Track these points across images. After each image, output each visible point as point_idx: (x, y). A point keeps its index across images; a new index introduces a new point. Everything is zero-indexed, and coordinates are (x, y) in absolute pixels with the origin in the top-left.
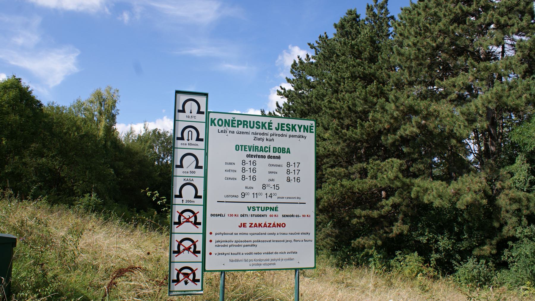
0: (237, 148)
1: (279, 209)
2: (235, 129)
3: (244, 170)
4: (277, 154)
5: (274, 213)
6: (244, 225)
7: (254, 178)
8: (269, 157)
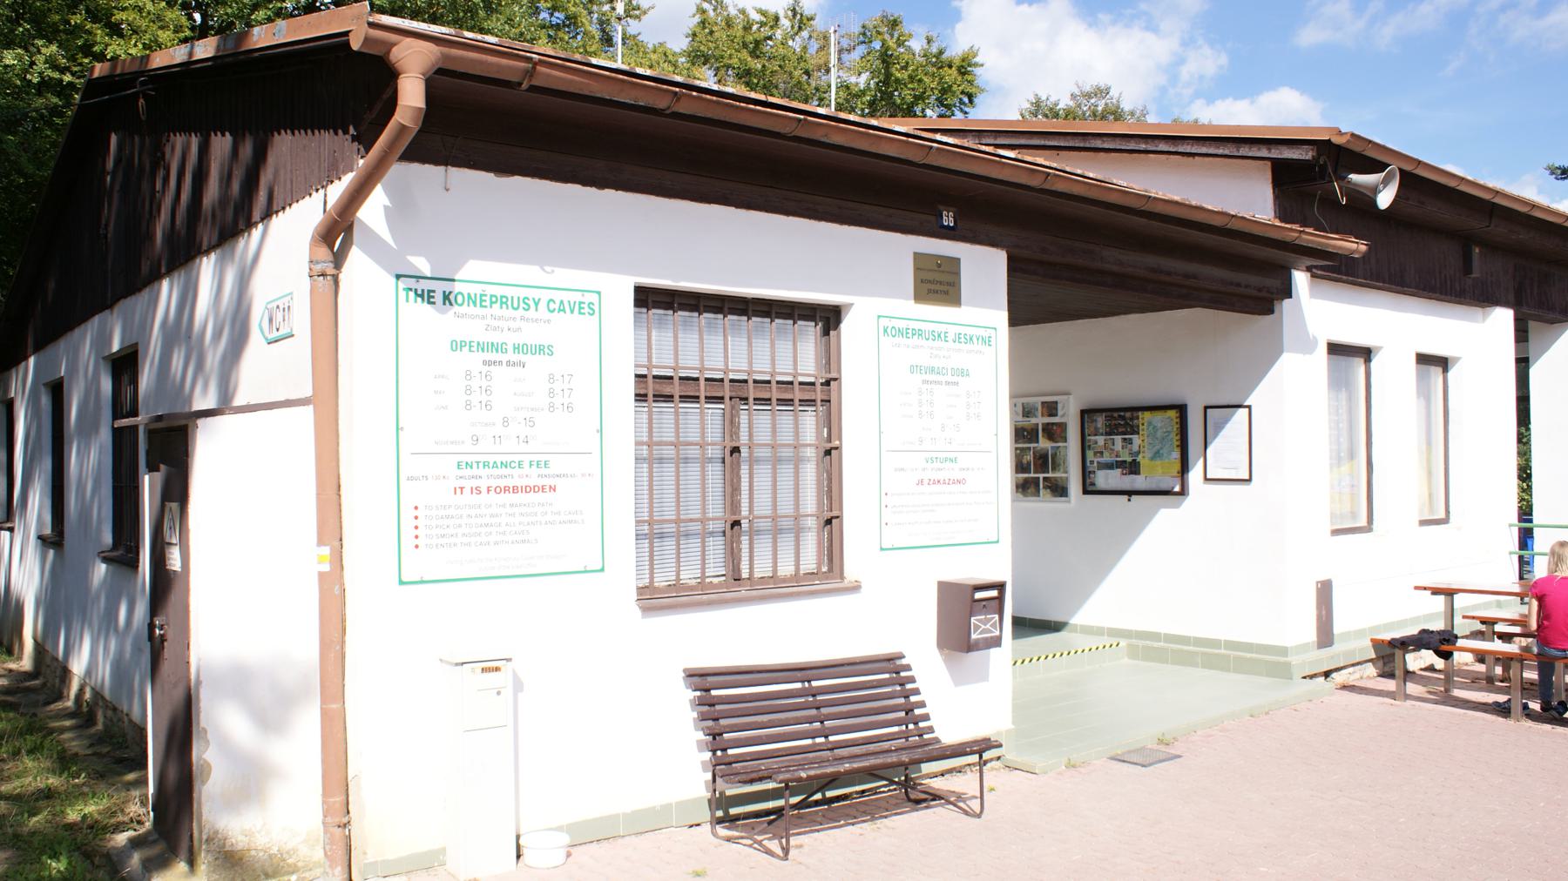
0: (457, 346)
1: (550, 464)
2: (909, 342)
3: (920, 404)
4: (955, 379)
5: (952, 465)
6: (921, 482)
7: (488, 406)
8: (948, 383)
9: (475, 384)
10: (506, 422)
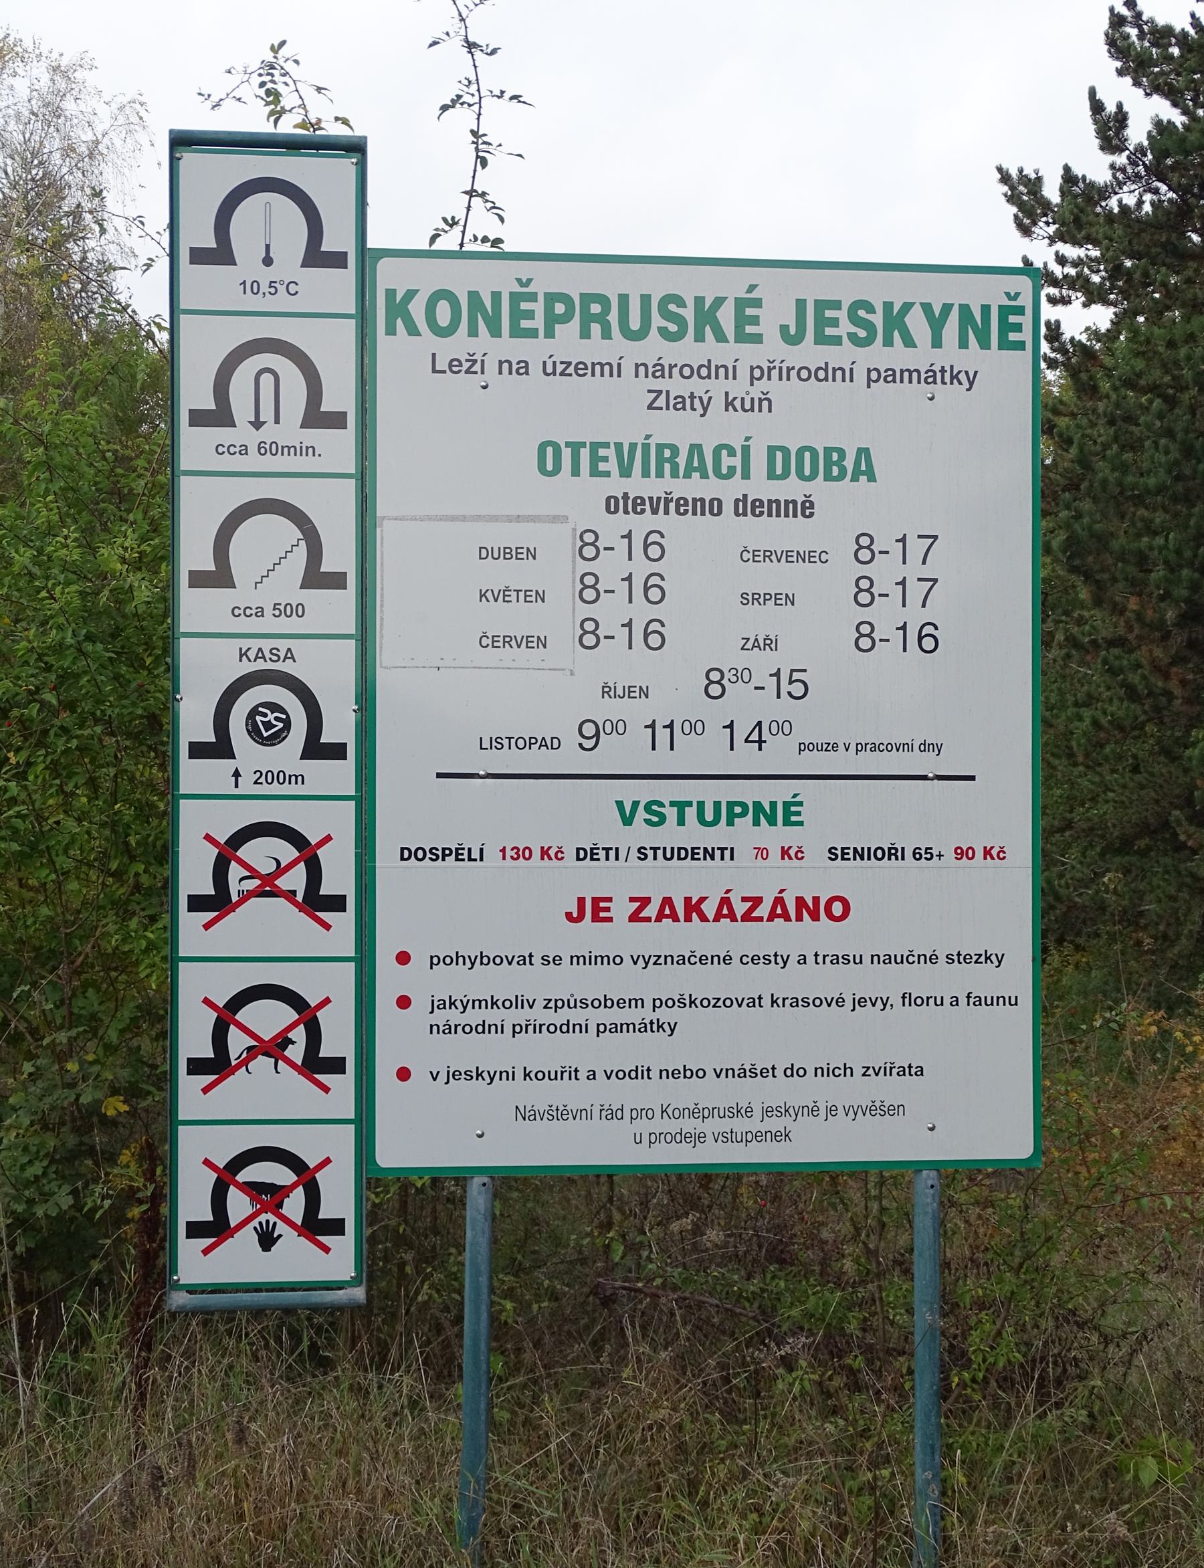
0: (549, 457)
2: (534, 351)
3: (589, 588)
5: (776, 836)
6: (599, 909)
7: (653, 636)
9: (610, 569)
10: (715, 683)
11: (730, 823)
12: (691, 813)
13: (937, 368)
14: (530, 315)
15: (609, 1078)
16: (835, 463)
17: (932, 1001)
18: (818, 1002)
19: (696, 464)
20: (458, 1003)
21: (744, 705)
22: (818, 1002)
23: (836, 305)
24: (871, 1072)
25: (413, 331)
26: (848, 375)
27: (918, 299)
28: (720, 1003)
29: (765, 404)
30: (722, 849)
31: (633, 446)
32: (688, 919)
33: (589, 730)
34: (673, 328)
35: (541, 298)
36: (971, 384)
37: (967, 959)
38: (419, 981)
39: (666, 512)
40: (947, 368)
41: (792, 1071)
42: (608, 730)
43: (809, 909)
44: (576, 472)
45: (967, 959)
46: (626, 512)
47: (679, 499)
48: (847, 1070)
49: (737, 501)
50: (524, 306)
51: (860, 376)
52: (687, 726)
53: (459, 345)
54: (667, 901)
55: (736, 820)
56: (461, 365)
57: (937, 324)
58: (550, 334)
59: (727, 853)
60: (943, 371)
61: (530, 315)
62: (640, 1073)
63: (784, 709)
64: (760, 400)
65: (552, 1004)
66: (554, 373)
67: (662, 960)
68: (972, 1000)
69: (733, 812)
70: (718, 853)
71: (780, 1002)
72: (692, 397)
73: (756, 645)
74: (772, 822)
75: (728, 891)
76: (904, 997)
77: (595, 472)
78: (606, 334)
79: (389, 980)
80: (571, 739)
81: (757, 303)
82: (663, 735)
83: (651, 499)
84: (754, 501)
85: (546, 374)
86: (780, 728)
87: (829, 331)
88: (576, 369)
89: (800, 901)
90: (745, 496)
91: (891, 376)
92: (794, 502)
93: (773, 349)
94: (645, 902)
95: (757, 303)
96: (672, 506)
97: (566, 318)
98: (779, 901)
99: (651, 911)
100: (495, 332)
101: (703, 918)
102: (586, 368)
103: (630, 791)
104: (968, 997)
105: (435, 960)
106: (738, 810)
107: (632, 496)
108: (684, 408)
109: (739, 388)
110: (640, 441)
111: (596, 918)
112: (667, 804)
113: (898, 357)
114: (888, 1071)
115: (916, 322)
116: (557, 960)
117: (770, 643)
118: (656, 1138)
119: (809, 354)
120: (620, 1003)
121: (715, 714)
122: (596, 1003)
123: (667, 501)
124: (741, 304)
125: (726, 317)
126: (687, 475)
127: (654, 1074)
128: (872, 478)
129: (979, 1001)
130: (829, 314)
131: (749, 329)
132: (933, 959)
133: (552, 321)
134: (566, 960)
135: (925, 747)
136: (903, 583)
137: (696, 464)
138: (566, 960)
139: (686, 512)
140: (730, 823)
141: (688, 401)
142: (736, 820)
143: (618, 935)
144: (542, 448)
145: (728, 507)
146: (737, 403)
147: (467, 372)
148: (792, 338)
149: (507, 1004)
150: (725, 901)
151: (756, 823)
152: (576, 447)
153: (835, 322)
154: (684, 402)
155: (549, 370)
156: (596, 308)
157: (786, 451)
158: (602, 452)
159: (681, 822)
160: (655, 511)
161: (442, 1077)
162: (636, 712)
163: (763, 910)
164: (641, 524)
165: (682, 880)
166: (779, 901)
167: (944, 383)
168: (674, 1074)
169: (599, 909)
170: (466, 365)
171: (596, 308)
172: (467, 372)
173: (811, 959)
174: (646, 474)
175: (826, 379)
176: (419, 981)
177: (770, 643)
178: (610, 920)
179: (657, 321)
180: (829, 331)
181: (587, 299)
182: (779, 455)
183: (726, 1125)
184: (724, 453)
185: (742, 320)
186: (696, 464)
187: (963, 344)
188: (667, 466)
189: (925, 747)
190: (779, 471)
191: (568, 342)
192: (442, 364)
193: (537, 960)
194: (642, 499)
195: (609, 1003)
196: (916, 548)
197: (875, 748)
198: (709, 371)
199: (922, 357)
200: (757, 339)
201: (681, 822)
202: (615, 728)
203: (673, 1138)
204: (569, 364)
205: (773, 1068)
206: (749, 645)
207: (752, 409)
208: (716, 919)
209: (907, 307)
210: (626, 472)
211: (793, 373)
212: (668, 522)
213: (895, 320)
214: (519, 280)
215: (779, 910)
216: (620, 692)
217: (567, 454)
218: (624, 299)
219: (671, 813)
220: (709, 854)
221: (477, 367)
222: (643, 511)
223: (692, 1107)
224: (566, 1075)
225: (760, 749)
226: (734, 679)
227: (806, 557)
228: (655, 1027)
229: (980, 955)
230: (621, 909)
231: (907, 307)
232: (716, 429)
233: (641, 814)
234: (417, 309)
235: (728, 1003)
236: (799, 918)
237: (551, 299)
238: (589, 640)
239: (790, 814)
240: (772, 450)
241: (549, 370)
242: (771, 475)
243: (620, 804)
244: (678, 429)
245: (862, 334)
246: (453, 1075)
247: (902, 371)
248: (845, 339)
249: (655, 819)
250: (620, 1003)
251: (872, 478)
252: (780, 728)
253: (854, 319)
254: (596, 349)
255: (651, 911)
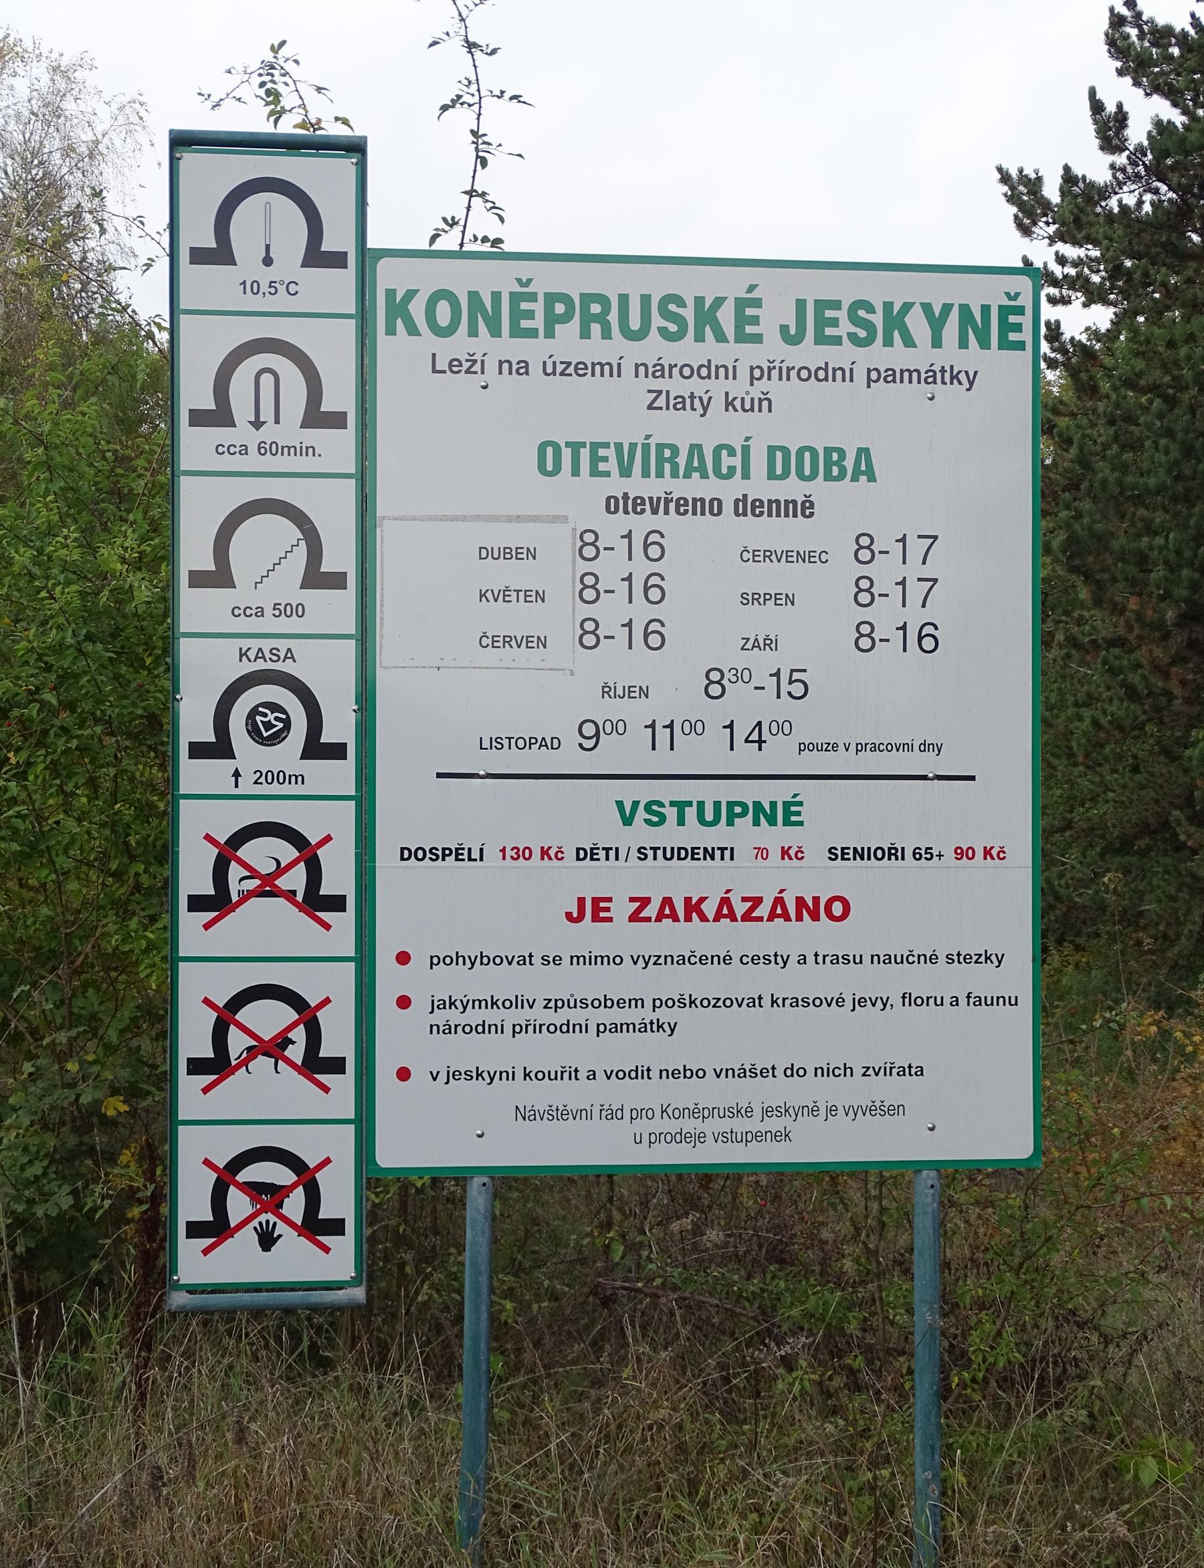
0: (549, 457)
2: (534, 351)
3: (589, 588)
5: (776, 836)
6: (599, 909)
7: (653, 636)
9: (610, 569)
10: (715, 683)
11: (730, 823)
12: (691, 813)
13: (937, 368)
14: (530, 315)
15: (609, 1078)
16: (835, 463)
17: (932, 1001)
18: (818, 1002)
19: (696, 464)
20: (458, 1003)
21: (744, 705)
22: (818, 1002)
23: (836, 305)
24: (871, 1072)
25: (413, 331)
26: (848, 375)
27: (918, 299)
28: (720, 1003)
29: (765, 404)
30: (722, 849)
31: (633, 446)
32: (688, 919)
33: (589, 730)
34: (673, 328)
35: (541, 298)
36: (971, 384)
37: (967, 959)
38: (419, 981)
39: (666, 512)
40: (947, 368)
41: (792, 1071)
42: (608, 730)
43: (809, 909)
44: (576, 472)
45: (967, 959)
46: (626, 512)
47: (679, 499)
48: (847, 1070)
49: (737, 501)
50: (524, 306)
51: (860, 376)
52: (687, 726)
53: (459, 345)
54: (667, 901)
55: (736, 820)
56: (461, 365)
57: (937, 324)
58: (550, 334)
59: (727, 853)
60: (943, 371)
61: (530, 315)
62: (640, 1073)
63: (784, 709)
64: (760, 400)
65: (552, 1004)
66: (554, 373)
67: (662, 960)
68: (972, 1000)
69: (733, 812)
70: (718, 853)
71: (780, 1002)
72: (692, 397)
73: (756, 645)
74: (772, 822)
75: (728, 891)
76: (904, 997)
77: (595, 472)
78: (606, 334)
79: (389, 980)
80: (571, 739)
81: (757, 303)
82: (663, 735)
83: (651, 499)
84: (754, 501)
85: (546, 374)
86: (780, 728)
87: (829, 331)
88: (576, 369)
89: (800, 901)
90: (745, 496)
91: (891, 376)
92: (794, 502)
93: (773, 349)
94: (645, 902)
95: (757, 303)
96: (672, 506)
97: (566, 318)
98: (779, 901)
99: (651, 911)
100: (495, 332)
101: (703, 918)
102: (586, 368)
103: (630, 791)
104: (968, 997)
105: (435, 960)
106: (738, 810)
107: (632, 496)
108: (684, 408)
109: (739, 388)
110: (640, 441)
111: (596, 918)
112: (667, 804)
113: (898, 357)
114: (888, 1071)
115: (916, 322)
116: (557, 960)
117: (770, 643)
118: (656, 1138)
119: (809, 354)
120: (620, 1003)
121: (715, 714)
122: (596, 1003)
123: (667, 501)
124: (741, 304)
125: (726, 317)
126: (687, 475)
127: (654, 1074)
128: (872, 478)
129: (979, 1001)
130: (829, 314)
131: (749, 329)
132: (933, 959)
133: (552, 321)
134: (566, 960)
135: (925, 747)
136: (903, 583)
137: (696, 464)
138: (566, 960)
139: (686, 512)
140: (730, 823)
141: (688, 401)
142: (736, 820)
143: (618, 935)
144: (542, 448)
145: (728, 507)
146: (737, 403)
147: (467, 372)
148: (792, 338)
149: (507, 1004)
150: (725, 901)
151: (756, 823)
152: (576, 447)
153: (835, 322)
154: (684, 402)
155: (549, 370)
156: (596, 308)
157: (786, 451)
158: (602, 452)
159: (681, 822)
160: (655, 511)
161: (442, 1077)
162: (636, 712)
163: (763, 910)
164: (641, 524)
165: (682, 880)
166: (779, 901)
167: (944, 383)
168: (674, 1074)
169: (599, 909)
170: (466, 365)
171: (596, 308)
172: (467, 372)
173: (811, 959)
174: (646, 474)
175: (826, 379)
176: (419, 981)
177: (770, 643)
178: (610, 920)
179: (657, 321)
180: (829, 331)
181: (587, 299)
182: (779, 455)
183: (726, 1125)
184: (724, 453)
185: (742, 320)
186: (696, 464)
187: (963, 344)
188: (667, 466)
189: (925, 747)
190: (779, 471)
191: (568, 342)
192: (442, 364)
193: (537, 960)
194: (642, 499)
195: (609, 1003)
196: (916, 548)
197: (875, 748)
198: (709, 371)
199: (922, 357)
200: (757, 339)
201: (681, 822)
202: (615, 728)
203: (673, 1138)
204: (569, 364)
205: (773, 1068)
206: (749, 645)
207: (752, 409)
208: (716, 919)
209: (907, 307)
210: (626, 472)
211: (793, 373)
212: (668, 522)
213: (895, 320)
214: (519, 280)
215: (779, 910)
216: (620, 692)
217: (567, 454)
218: (624, 299)
219: (671, 813)
220: (709, 854)
221: (477, 367)
222: (643, 511)
223: (692, 1107)
224: (566, 1075)
225: (760, 749)
226: (734, 679)
227: (806, 557)
228: (655, 1027)
229: (980, 955)
230: (621, 909)
231: (907, 307)
232: (716, 429)
233: (641, 814)
234: (417, 309)
235: (728, 1003)
236: (799, 918)
237: (551, 299)
238: (589, 640)
239: (790, 814)
240: (772, 450)
241: (549, 370)
242: (771, 475)
243: (620, 804)
244: (678, 429)
245: (862, 334)
246: (453, 1075)
247: (902, 371)
248: (845, 339)
249: (655, 819)
250: (620, 1003)
251: (872, 478)
252: (780, 728)
253: (854, 319)
254: (596, 349)
255: (651, 911)
